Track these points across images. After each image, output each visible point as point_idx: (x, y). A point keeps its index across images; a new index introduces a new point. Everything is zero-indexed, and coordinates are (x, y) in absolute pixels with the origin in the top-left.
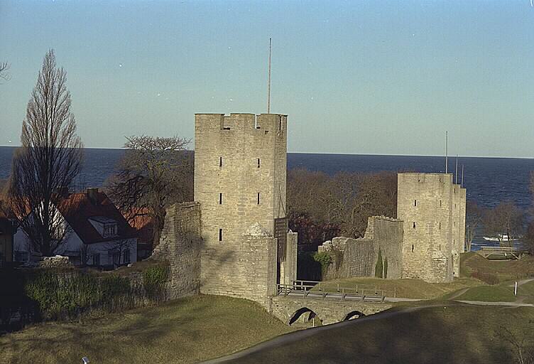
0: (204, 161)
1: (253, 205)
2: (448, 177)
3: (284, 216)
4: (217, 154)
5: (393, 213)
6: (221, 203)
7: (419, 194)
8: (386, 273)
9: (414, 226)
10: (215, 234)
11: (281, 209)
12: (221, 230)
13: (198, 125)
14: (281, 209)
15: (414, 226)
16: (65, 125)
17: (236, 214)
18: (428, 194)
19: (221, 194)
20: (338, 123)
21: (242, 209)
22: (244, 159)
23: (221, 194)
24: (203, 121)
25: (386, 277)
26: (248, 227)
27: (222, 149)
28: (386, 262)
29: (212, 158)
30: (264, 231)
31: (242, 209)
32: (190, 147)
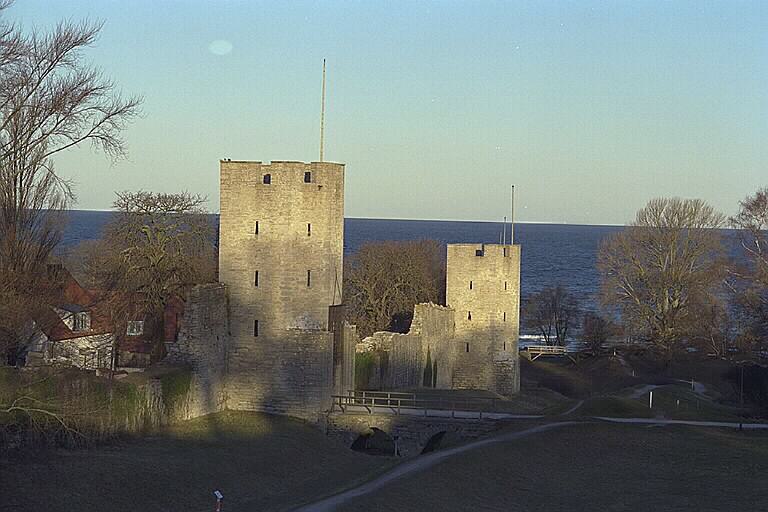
0: (233, 227)
1: (301, 287)
2: (515, 251)
3: (340, 303)
4: (252, 217)
5: (441, 299)
6: (256, 285)
7: (476, 272)
8: (435, 382)
9: (470, 318)
10: (249, 282)
11: (337, 292)
12: (256, 321)
13: (224, 177)
14: (337, 292)
15: (470, 318)
16: (39, 176)
17: (278, 300)
18: (488, 272)
19: (257, 273)
20: (388, 192)
21: (286, 294)
22: (289, 224)
23: (257, 273)
24: (233, 171)
25: (435, 386)
26: (294, 317)
27: (258, 209)
28: (435, 365)
29: (245, 222)
30: (207, 387)
31: (286, 294)
32: (210, 207)
